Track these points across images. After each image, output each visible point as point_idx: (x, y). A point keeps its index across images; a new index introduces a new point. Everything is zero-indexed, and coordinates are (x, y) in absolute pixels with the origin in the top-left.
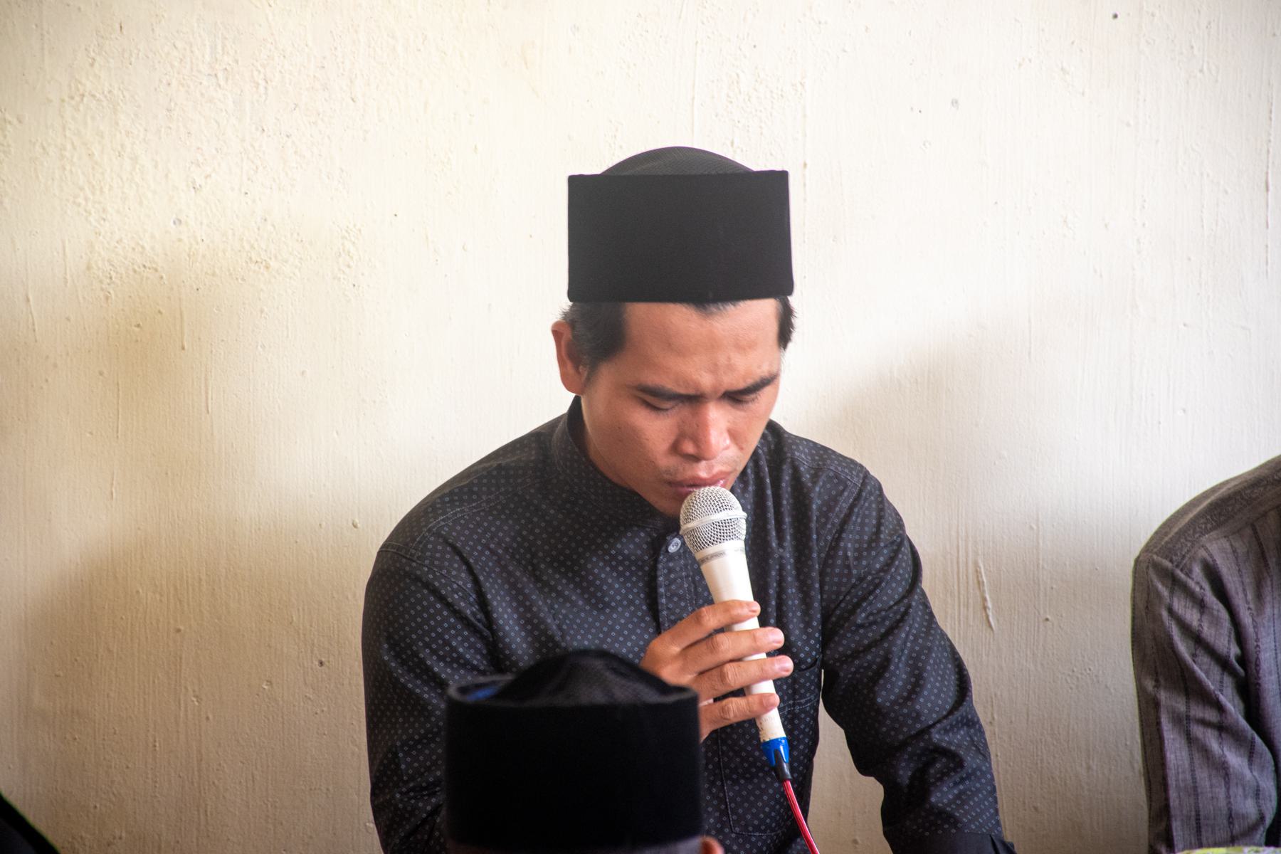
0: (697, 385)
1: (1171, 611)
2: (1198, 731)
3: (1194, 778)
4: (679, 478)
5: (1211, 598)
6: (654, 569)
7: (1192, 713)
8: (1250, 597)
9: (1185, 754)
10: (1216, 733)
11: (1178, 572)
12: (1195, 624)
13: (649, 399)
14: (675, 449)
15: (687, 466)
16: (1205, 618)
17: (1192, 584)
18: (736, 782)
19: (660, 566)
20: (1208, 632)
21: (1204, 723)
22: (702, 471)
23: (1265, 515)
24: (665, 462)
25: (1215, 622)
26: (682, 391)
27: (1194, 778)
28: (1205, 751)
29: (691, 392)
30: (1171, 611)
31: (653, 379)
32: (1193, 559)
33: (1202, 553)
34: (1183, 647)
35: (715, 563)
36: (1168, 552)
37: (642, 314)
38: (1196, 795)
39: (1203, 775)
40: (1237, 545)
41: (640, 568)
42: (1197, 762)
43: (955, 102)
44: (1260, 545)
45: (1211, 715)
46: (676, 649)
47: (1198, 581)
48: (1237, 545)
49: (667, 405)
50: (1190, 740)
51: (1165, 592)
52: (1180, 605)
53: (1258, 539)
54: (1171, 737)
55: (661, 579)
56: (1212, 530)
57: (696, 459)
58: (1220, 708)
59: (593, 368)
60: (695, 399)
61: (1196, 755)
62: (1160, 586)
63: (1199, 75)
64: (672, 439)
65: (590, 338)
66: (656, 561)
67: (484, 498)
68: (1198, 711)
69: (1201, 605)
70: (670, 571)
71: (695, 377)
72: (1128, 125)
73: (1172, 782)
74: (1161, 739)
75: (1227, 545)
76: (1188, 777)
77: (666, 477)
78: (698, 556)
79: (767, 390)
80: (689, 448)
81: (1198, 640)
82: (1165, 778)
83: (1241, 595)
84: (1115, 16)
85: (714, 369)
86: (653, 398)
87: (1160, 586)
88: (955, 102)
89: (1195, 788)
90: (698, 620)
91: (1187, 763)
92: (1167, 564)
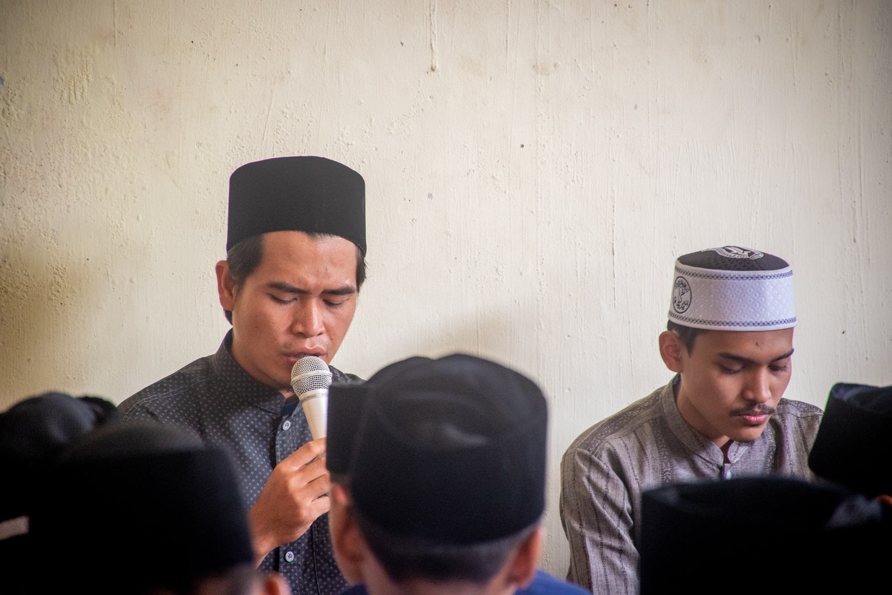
0: (306, 283)
1: (589, 479)
2: (608, 553)
3: (607, 580)
4: (292, 349)
5: (612, 473)
6: (274, 440)
7: (604, 541)
8: (636, 473)
9: (601, 566)
10: (618, 555)
11: (593, 456)
12: (604, 487)
13: (275, 292)
14: (291, 330)
15: (297, 341)
16: (610, 485)
17: (602, 464)
18: (324, 579)
19: (278, 438)
20: (611, 493)
21: (611, 548)
22: (307, 344)
23: (641, 426)
24: (283, 338)
25: (616, 487)
26: (297, 286)
27: (607, 580)
28: (612, 565)
29: (301, 287)
30: (589, 479)
31: (278, 279)
32: (602, 449)
33: (607, 446)
34: (598, 503)
35: (312, 401)
36: (586, 445)
37: (273, 240)
38: (608, 589)
39: (611, 578)
40: (627, 442)
41: (264, 439)
42: (608, 571)
43: (430, 196)
44: (640, 443)
45: (616, 543)
46: (296, 468)
47: (605, 462)
48: (627, 442)
49: (288, 297)
50: (604, 559)
51: (585, 469)
52: (595, 476)
53: (638, 439)
54: (593, 555)
55: (278, 446)
56: (612, 433)
57: (304, 335)
58: (620, 538)
59: (241, 283)
60: (302, 294)
61: (607, 567)
62: (582, 465)
63: (572, 183)
64: (289, 323)
65: (240, 268)
66: (275, 434)
67: (171, 391)
68: (607, 541)
69: (607, 476)
70: (283, 442)
71: (305, 277)
72: (532, 212)
73: (594, 581)
74: (587, 556)
75: (621, 442)
76: (604, 579)
77: (284, 350)
78: (301, 397)
79: (346, 297)
80: (300, 328)
81: (606, 498)
82: (590, 579)
83: (631, 471)
84: (522, 146)
85: (317, 274)
86: (278, 291)
87: (582, 465)
88: (430, 196)
89: (607, 585)
90: (309, 449)
91: (602, 571)
92: (586, 452)
